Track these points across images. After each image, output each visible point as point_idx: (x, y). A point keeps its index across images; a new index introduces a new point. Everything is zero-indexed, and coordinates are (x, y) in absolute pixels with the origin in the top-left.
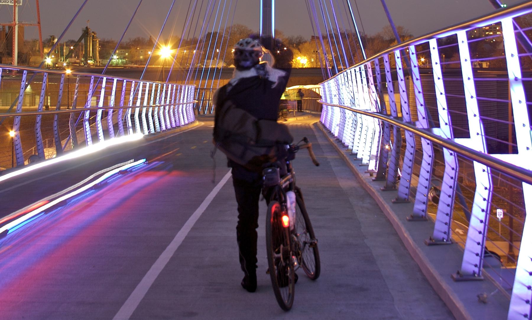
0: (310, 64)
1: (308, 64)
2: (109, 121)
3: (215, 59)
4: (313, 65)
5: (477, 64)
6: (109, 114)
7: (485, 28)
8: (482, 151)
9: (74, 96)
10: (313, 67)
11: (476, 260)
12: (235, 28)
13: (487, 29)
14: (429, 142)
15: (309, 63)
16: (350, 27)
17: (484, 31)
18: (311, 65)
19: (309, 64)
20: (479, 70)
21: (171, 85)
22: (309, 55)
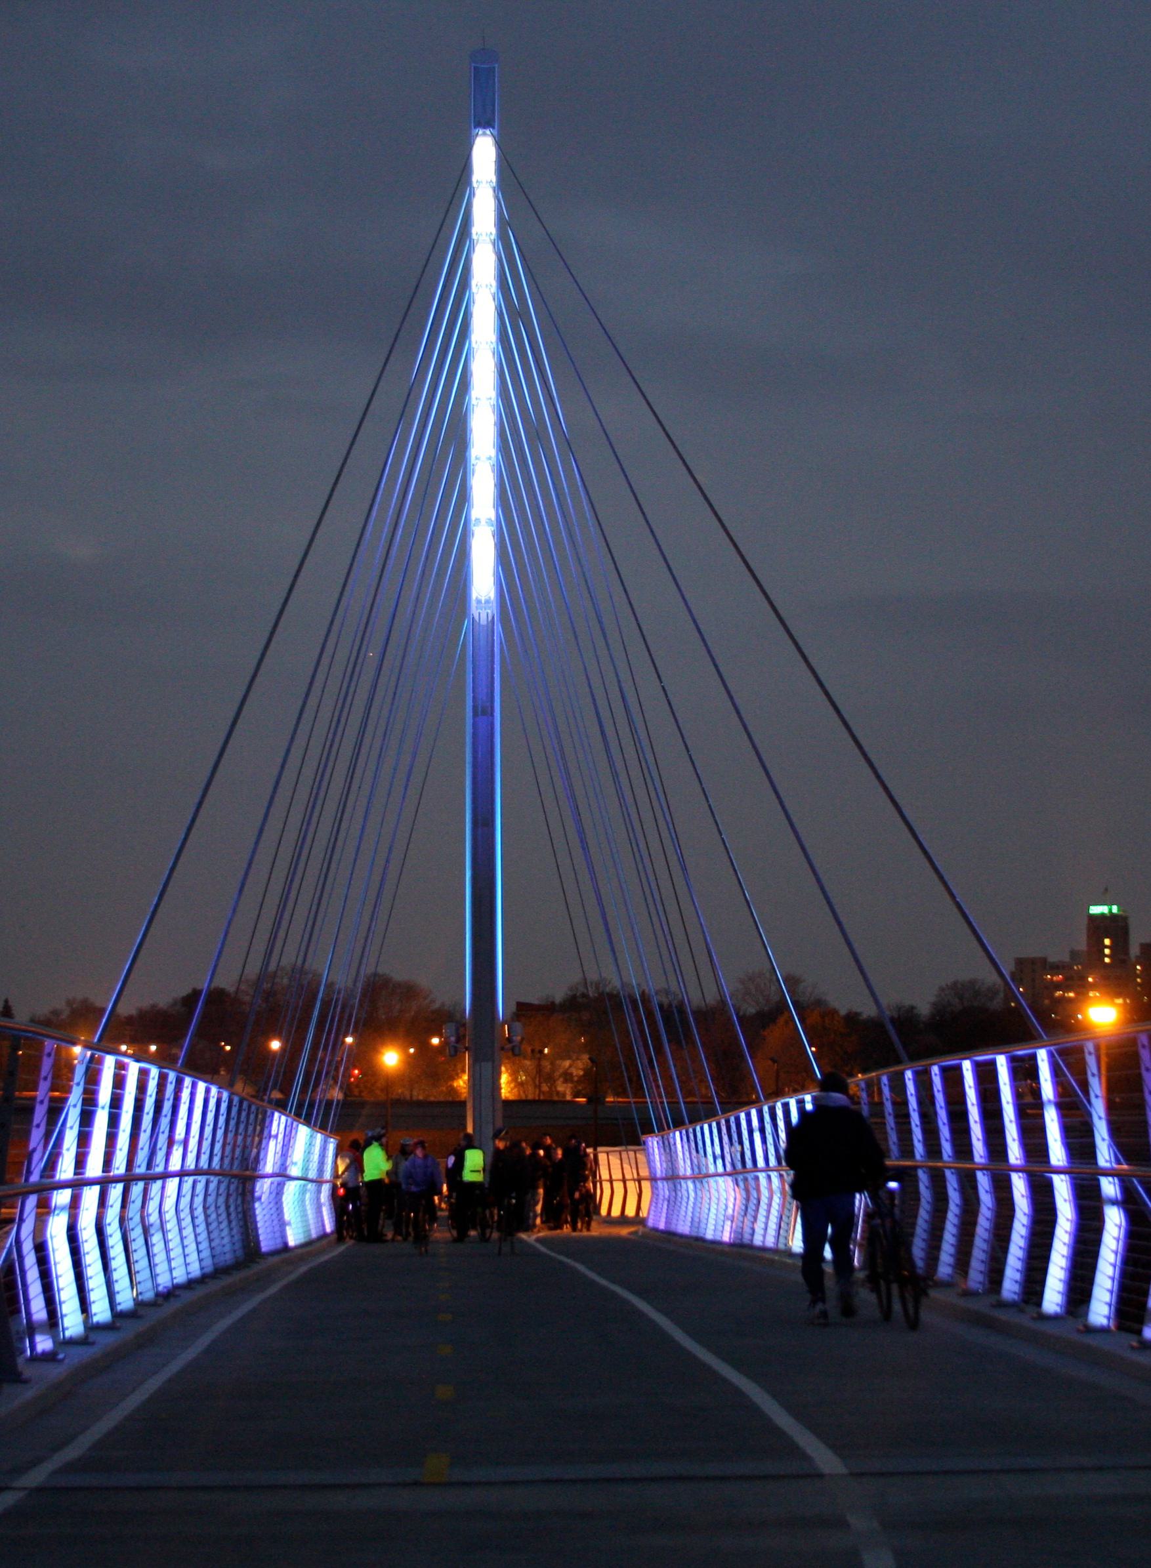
0: (516, 1090)
1: (509, 1089)
2: (167, 1215)
3: (222, 1073)
4: (524, 1092)
5: (1026, 1090)
6: (110, 1203)
7: (1052, 979)
8: (964, 976)
9: (862, 1080)
10: (524, 1097)
11: (1016, 1288)
12: (282, 979)
13: (1058, 981)
14: (953, 1170)
15: (512, 1085)
16: (668, 983)
17: (1046, 988)
18: (519, 1091)
19: (512, 1089)
20: (1031, 1109)
21: (916, 1074)
22: (514, 1063)
